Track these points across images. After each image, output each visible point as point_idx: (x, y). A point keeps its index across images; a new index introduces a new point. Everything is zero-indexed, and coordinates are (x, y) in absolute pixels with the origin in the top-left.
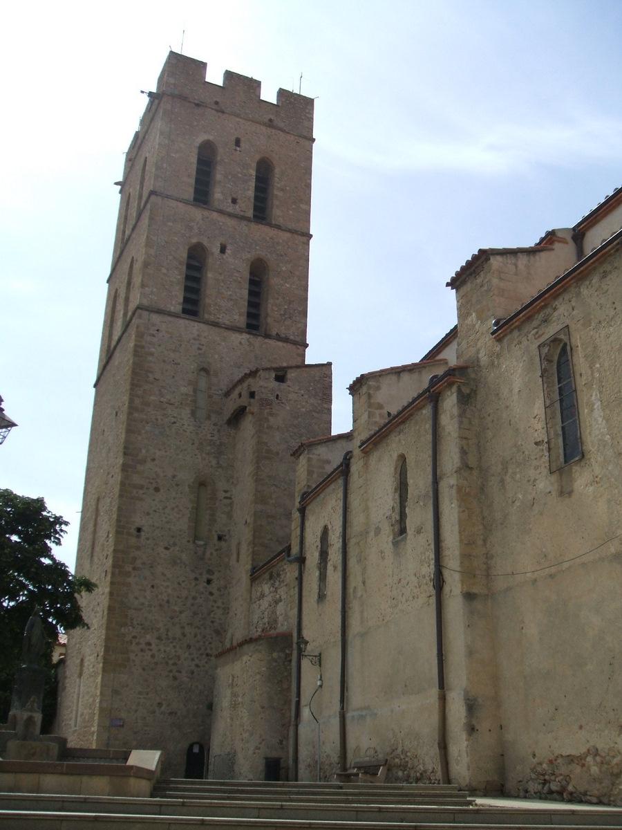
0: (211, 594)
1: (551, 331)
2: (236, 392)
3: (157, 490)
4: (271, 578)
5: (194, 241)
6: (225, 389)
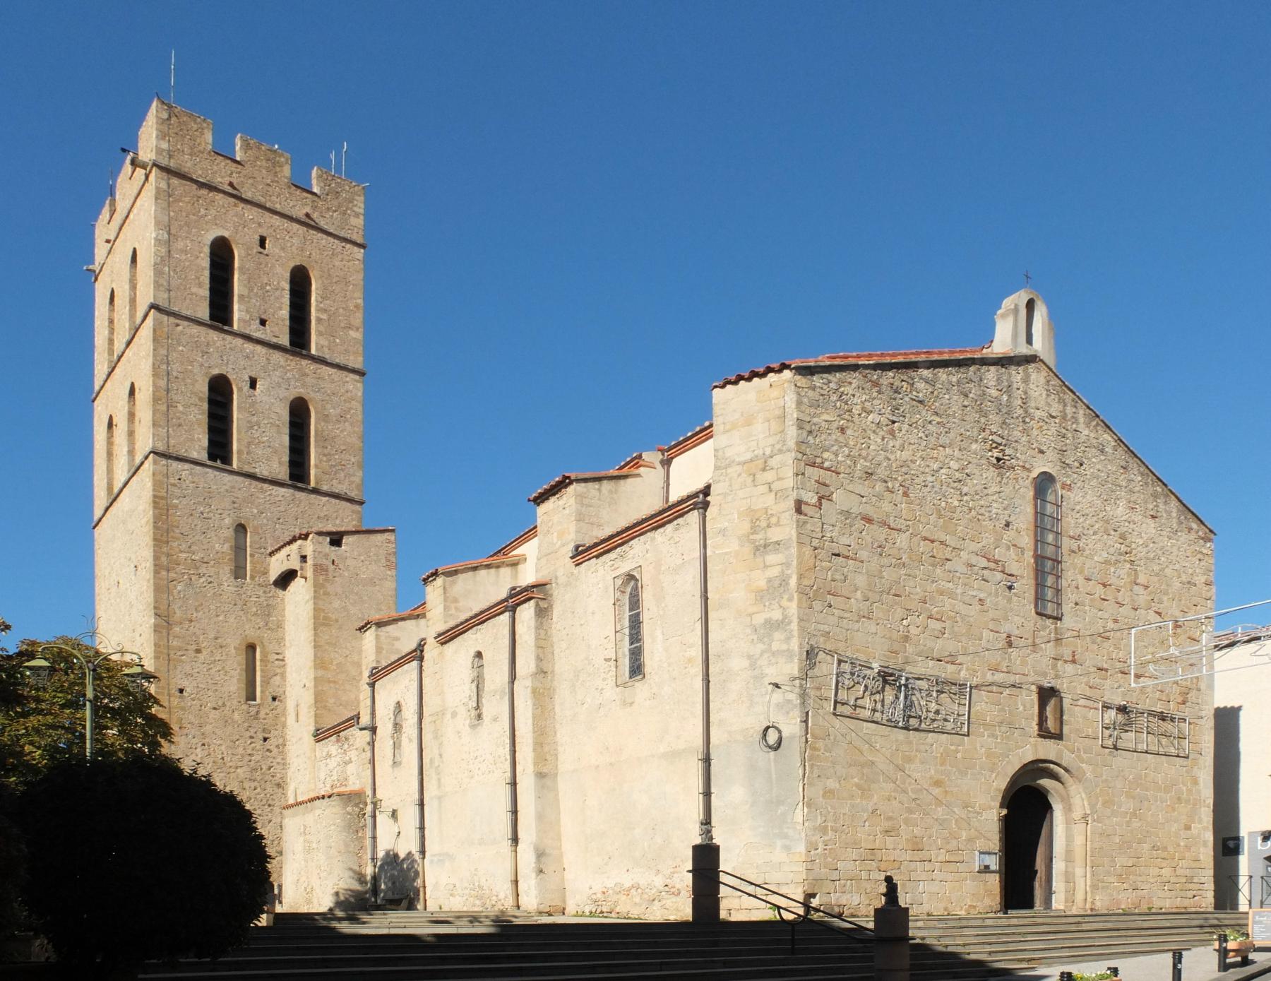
1: (626, 567)
3: (198, 651)
4: (338, 741)
5: (216, 371)
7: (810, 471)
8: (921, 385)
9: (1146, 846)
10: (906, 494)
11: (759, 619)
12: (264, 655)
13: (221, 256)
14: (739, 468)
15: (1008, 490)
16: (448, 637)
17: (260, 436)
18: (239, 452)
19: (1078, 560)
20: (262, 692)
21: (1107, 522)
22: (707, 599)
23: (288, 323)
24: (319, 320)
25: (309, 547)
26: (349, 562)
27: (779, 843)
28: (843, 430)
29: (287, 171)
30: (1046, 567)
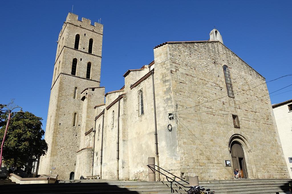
0: (77, 138)
1: (140, 88)
2: (83, 93)
3: (65, 115)
5: (74, 58)
6: (81, 92)
7: (173, 64)
8: (195, 47)
9: (268, 159)
10: (195, 69)
11: (165, 98)
12: (78, 115)
13: (78, 37)
14: (159, 65)
15: (218, 68)
16: (108, 108)
17: (81, 69)
18: (77, 73)
19: (236, 84)
20: (77, 124)
21: (240, 76)
22: (154, 94)
23: (88, 48)
24: (94, 48)
25: (87, 91)
26: (95, 94)
27: (174, 158)
28: (180, 56)
29: (90, 23)
30: (229, 86)
